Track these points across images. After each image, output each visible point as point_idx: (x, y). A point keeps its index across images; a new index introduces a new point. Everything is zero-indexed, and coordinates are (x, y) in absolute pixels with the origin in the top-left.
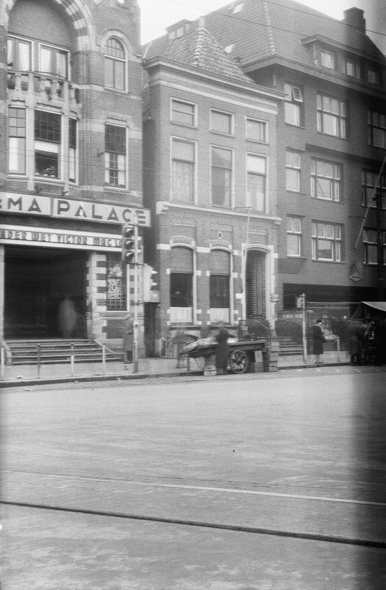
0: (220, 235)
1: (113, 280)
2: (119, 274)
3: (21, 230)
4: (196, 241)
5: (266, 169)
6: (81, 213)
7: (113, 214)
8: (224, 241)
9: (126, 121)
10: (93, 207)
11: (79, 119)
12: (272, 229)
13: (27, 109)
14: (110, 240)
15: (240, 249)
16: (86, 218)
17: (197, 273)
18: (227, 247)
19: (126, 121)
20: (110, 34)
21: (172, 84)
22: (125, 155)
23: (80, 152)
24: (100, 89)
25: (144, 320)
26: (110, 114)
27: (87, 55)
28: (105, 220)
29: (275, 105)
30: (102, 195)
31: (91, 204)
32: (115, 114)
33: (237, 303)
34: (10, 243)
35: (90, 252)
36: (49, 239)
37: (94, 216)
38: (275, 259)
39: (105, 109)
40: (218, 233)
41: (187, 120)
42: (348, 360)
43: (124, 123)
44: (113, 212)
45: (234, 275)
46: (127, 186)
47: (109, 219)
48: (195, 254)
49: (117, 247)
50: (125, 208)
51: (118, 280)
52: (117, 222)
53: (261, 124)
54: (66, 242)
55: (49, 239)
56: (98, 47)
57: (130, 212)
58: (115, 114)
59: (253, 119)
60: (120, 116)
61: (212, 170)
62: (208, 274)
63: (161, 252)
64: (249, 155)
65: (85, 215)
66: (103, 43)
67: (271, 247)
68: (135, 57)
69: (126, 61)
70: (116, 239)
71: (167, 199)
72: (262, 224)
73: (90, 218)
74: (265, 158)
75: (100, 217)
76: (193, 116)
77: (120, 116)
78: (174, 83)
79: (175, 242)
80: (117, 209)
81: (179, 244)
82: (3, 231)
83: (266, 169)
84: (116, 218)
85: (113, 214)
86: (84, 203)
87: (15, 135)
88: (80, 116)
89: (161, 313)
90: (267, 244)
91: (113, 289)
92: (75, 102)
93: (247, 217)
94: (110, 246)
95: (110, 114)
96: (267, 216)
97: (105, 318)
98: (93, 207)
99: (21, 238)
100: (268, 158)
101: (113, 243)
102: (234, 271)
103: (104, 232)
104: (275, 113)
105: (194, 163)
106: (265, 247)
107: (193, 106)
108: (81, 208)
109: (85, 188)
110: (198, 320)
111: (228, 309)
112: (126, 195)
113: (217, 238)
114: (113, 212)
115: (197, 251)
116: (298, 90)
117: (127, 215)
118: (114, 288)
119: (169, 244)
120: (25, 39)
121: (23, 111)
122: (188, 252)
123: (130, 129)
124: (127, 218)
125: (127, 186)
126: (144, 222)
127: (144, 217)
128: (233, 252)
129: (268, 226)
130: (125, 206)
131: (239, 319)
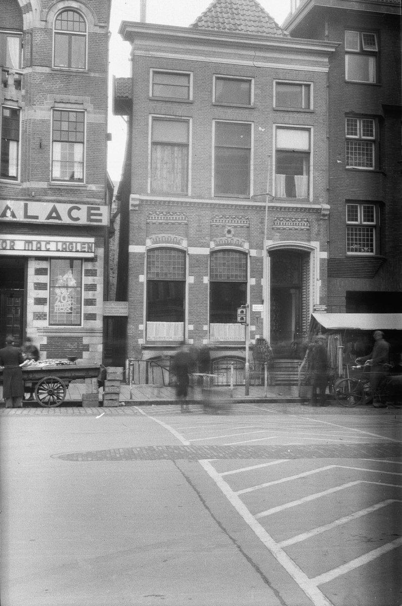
0: (229, 232)
1: (64, 290)
2: (73, 283)
3: (80, 241)
4: (249, 242)
5: (310, 144)
6: (9, 213)
7: (54, 213)
8: (235, 239)
9: (82, 104)
10: (26, 205)
11: (21, 108)
12: (318, 221)
13: (86, 113)
14: (48, 243)
15: (260, 247)
16: (15, 219)
17: (190, 280)
18: (241, 246)
19: (82, 104)
20: (61, 5)
21: (151, 53)
22: (18, 141)
23: (23, 145)
24: (46, 70)
25: (103, 336)
26: (58, 97)
27: (31, 34)
28: (42, 219)
29: (326, 60)
30: (45, 192)
31: (22, 203)
32: (65, 97)
33: (257, 318)
34: (7, 254)
35: (25, 259)
36: (57, 245)
37: (26, 216)
38: (322, 260)
39: (51, 92)
40: (227, 230)
41: (180, 94)
42: (173, 398)
43: (81, 106)
44: (54, 210)
45: (252, 282)
46: (19, 178)
47: (47, 219)
48: (187, 256)
49: (58, 251)
50: (71, 205)
51: (70, 290)
52: (60, 222)
53: (303, 87)
54: (30, 249)
55: (57, 245)
56: (44, 23)
57: (79, 209)
58: (65, 97)
59: (162, 70)
60: (73, 98)
61: (215, 150)
62: (206, 280)
63: (130, 256)
64: (278, 127)
65: (13, 215)
66: (52, 17)
67: (315, 244)
68: (98, 28)
69: (87, 34)
70: (57, 242)
71: (142, 191)
72: (302, 215)
73: (20, 218)
74: (309, 130)
75: (37, 217)
76: (189, 87)
77: (73, 98)
78: (153, 50)
79: (154, 243)
80: (59, 207)
81: (223, 247)
82: (4, 241)
83: (310, 144)
84: (59, 217)
85: (54, 213)
86: (13, 202)
87: (59, 139)
88: (22, 104)
89: (131, 329)
90: (309, 241)
91: (62, 301)
92: (14, 88)
93: (265, 207)
94: (48, 250)
95: (58, 97)
96: (310, 203)
97: (45, 334)
98: (26, 205)
99: (86, 251)
100: (312, 130)
101: (52, 246)
102: (252, 277)
103: (70, 236)
104: (326, 70)
105: (310, 153)
106: (304, 244)
107: (188, 75)
108: (7, 208)
109: (26, 185)
110: (190, 338)
111: (183, 323)
112: (79, 190)
113: (224, 236)
114: (54, 210)
115: (189, 253)
116: (373, 36)
117: (75, 213)
118: (64, 300)
119: (144, 245)
120: (6, 32)
121: (82, 114)
122: (181, 254)
123: (88, 112)
124: (74, 216)
125: (19, 178)
126: (100, 221)
127: (100, 215)
128: (249, 252)
129: (312, 217)
130: (71, 202)
131: (257, 337)
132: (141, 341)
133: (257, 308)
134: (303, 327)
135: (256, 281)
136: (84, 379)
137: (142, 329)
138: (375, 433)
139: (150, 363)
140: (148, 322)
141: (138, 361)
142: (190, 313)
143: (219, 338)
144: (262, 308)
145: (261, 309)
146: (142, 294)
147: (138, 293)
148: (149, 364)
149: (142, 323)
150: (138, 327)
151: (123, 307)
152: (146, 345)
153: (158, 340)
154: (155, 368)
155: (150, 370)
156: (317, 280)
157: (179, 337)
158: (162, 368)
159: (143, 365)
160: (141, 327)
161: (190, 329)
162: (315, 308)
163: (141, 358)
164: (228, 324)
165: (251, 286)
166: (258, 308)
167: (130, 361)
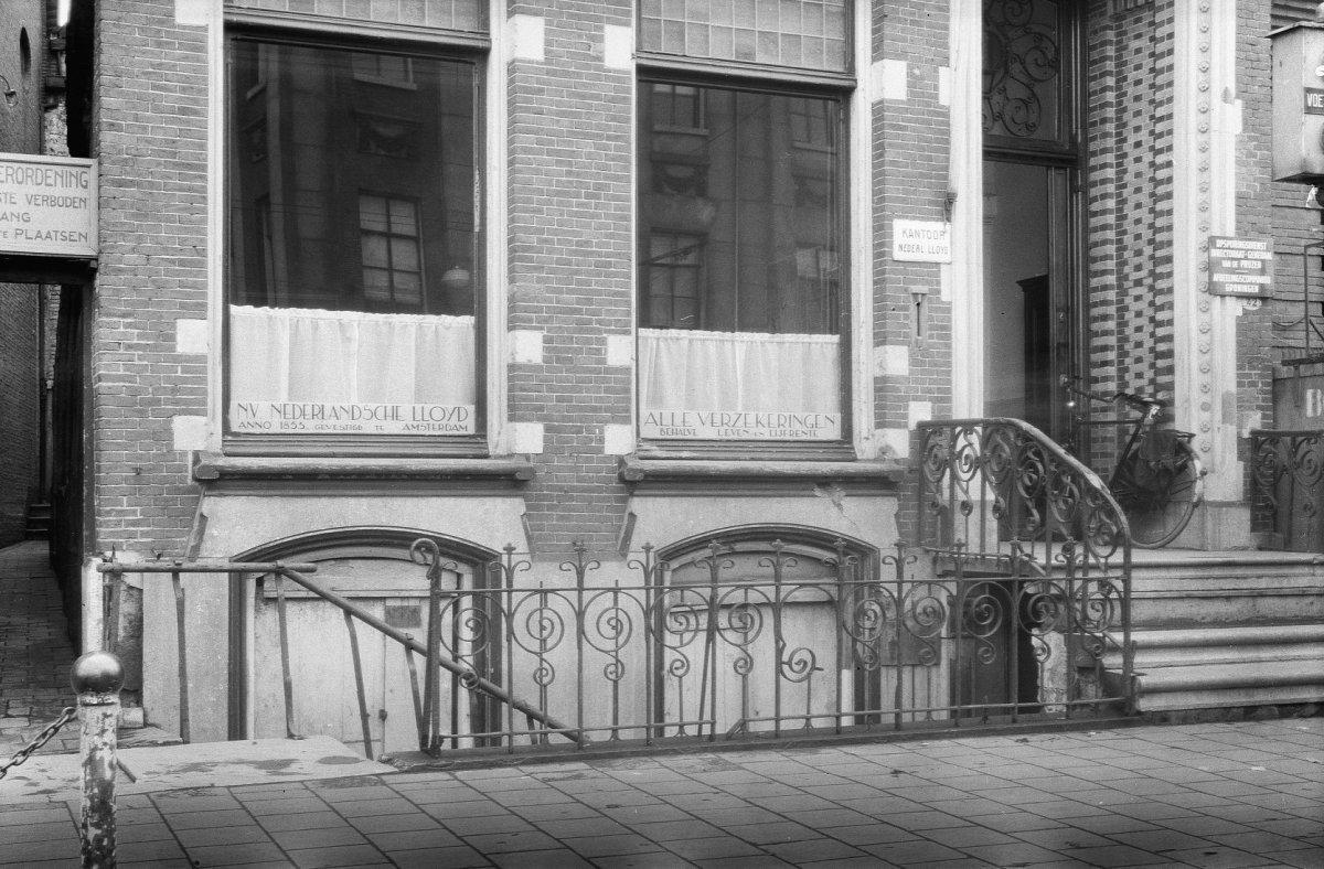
62: (619, 49)
111: (468, 321)
131: (921, 412)
132: (194, 436)
133: (914, 238)
134: (1099, 432)
135: (913, 82)
136: (368, 715)
137: (199, 348)
138: (54, 474)
139: (260, 582)
140: (234, 309)
141: (176, 573)
142: (515, 253)
143: (693, 420)
144: (945, 242)
145: (940, 249)
146: (191, 111)
147: (172, 99)
148: (251, 585)
149: (199, 310)
150: (172, 338)
151: (58, 191)
152: (223, 462)
153: (311, 426)
154: (292, 610)
155: (259, 626)
156: (1225, 97)
157: (448, 410)
158: (349, 613)
159: (208, 596)
160: (195, 336)
161: (521, 359)
162: (1215, 253)
163: (196, 549)
164: (747, 336)
165: (879, 110)
166: (924, 242)
167: (115, 574)
